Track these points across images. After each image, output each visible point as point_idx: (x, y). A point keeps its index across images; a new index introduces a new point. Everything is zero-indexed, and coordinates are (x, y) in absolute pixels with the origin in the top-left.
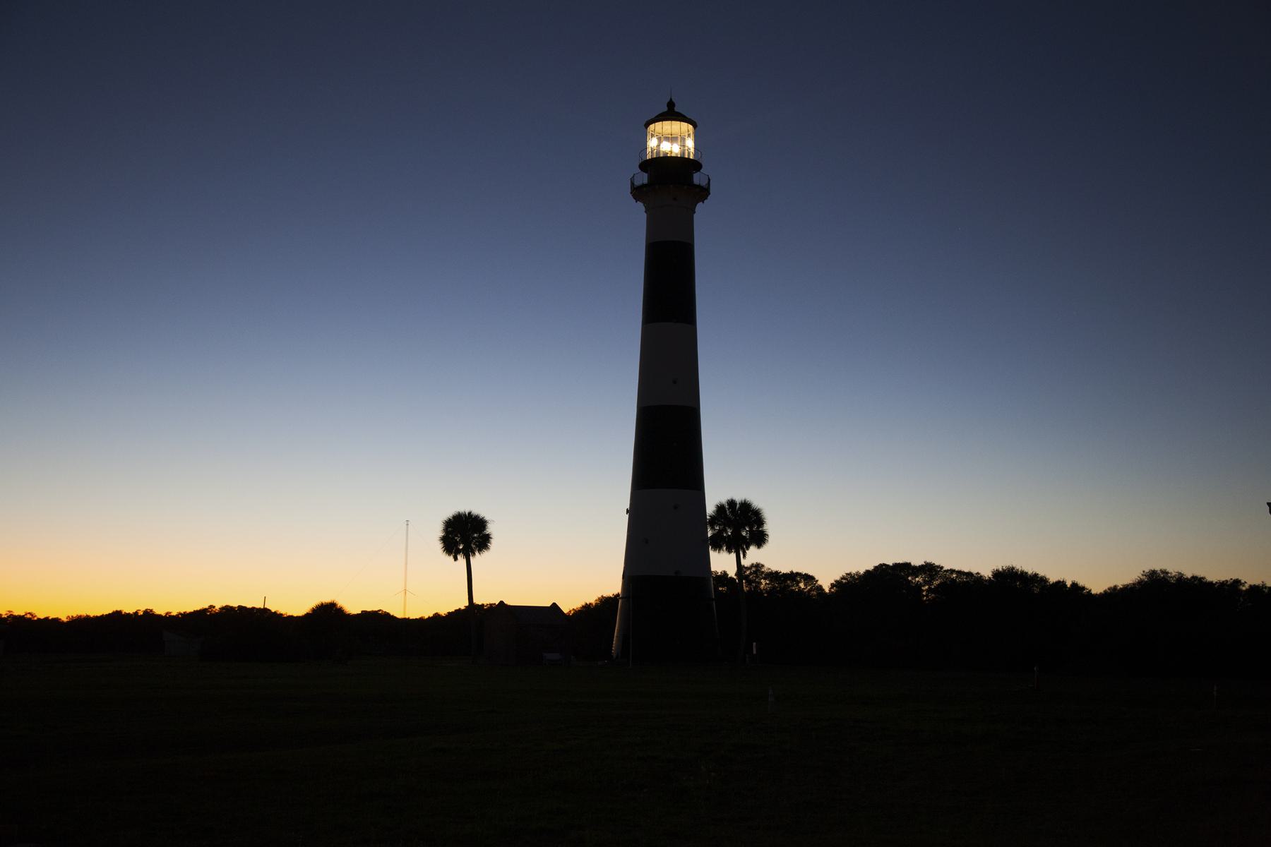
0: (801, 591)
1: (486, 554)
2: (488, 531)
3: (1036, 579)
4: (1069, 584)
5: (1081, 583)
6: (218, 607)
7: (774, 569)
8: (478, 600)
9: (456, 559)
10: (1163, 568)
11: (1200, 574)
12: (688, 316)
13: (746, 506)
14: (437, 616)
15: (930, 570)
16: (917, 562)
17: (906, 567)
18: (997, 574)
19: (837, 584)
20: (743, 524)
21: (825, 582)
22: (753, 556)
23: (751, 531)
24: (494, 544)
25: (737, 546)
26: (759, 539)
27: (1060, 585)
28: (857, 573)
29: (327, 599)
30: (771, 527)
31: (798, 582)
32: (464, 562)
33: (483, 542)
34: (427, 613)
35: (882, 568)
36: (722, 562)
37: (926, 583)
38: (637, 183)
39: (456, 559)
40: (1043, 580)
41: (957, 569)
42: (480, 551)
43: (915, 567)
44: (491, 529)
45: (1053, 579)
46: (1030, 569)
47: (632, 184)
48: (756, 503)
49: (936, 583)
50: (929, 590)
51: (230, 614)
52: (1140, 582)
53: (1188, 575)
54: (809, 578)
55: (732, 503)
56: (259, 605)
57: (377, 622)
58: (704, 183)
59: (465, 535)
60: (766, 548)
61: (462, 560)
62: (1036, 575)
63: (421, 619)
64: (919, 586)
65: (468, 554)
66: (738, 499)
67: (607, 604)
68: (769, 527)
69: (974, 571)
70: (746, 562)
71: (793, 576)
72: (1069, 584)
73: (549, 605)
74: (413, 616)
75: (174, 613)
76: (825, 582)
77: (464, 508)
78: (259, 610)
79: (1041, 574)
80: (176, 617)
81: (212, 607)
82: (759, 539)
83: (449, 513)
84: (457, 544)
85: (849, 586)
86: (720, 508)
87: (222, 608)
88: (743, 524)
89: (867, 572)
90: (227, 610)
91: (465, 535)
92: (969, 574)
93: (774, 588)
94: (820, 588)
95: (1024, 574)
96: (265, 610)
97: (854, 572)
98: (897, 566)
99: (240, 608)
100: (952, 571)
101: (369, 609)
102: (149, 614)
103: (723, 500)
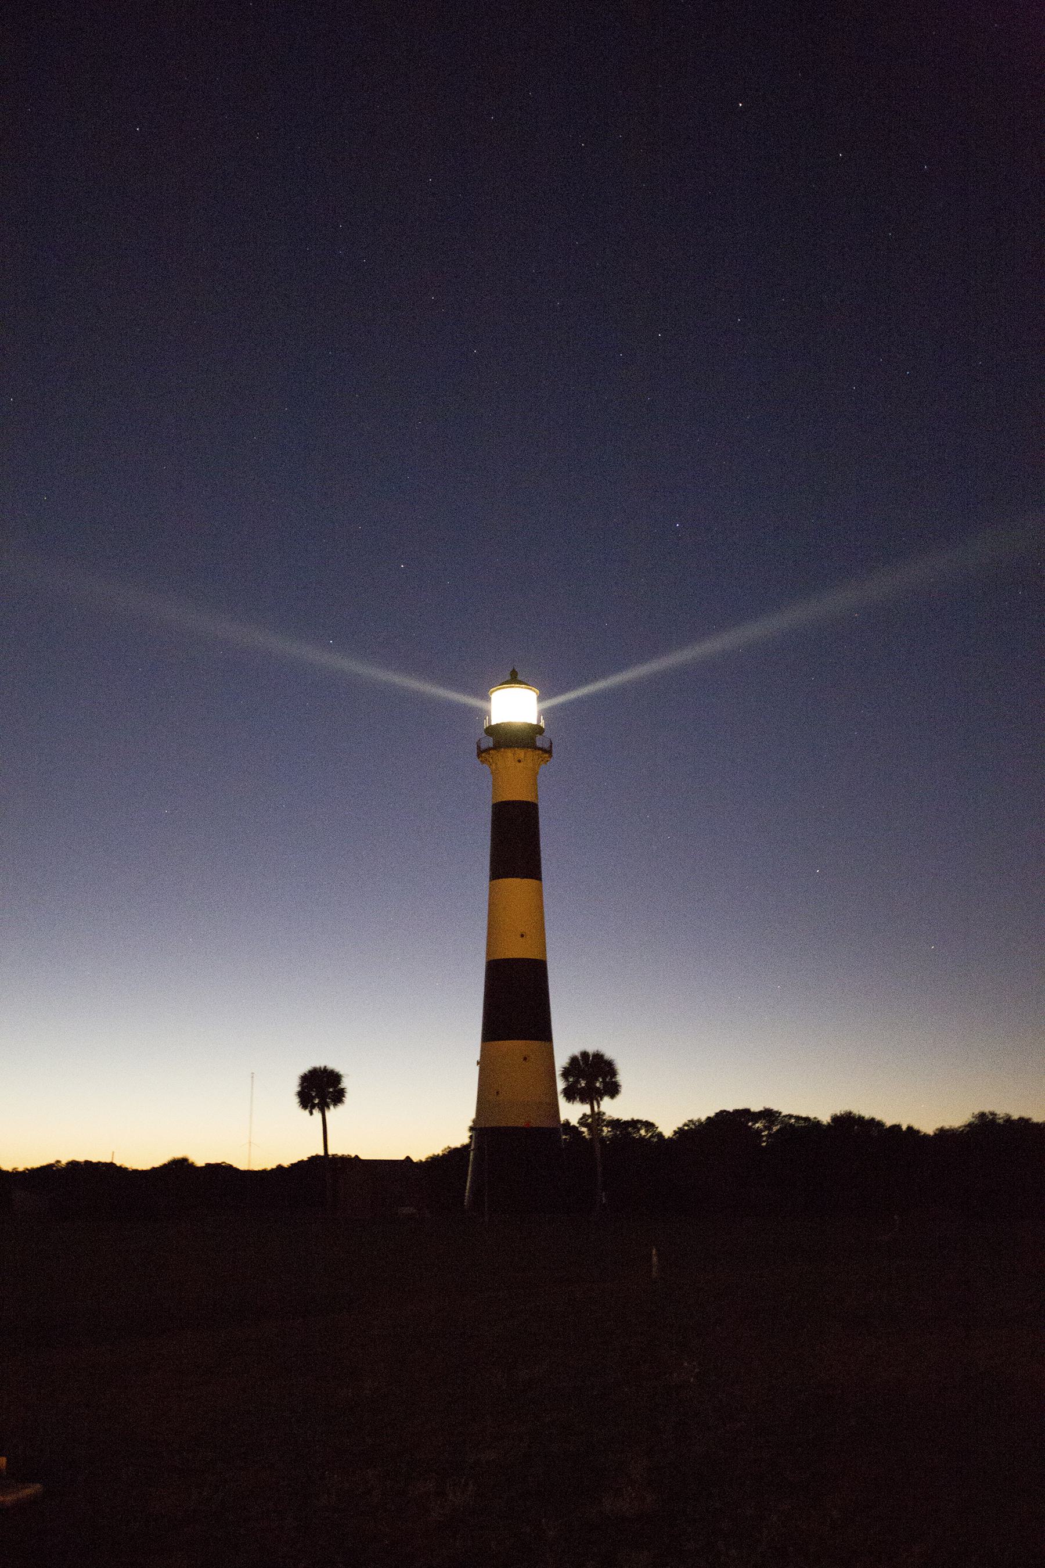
0: (642, 1138)
1: (340, 1107)
2: (343, 1085)
3: (874, 1124)
4: (904, 1128)
5: (916, 1127)
6: (64, 1162)
7: (616, 1116)
8: (331, 1151)
9: (311, 1113)
10: (991, 1109)
11: (1026, 1116)
12: (531, 869)
13: (598, 1057)
14: (280, 1168)
15: (768, 1115)
16: (756, 1107)
17: (746, 1112)
18: (836, 1119)
19: (680, 1132)
20: (595, 1075)
21: (668, 1132)
22: (612, 1108)
23: (604, 1081)
24: (348, 1098)
25: (590, 1096)
26: (613, 1090)
27: (896, 1128)
28: (699, 1120)
29: (179, 1155)
30: (623, 1078)
31: (639, 1130)
32: (320, 1115)
33: (338, 1097)
34: (270, 1165)
35: (722, 1115)
36: (571, 1112)
37: (766, 1128)
38: (483, 746)
39: (311, 1113)
40: (879, 1124)
41: (795, 1113)
42: (335, 1105)
43: (754, 1113)
44: (345, 1083)
45: (889, 1122)
46: (867, 1114)
47: (479, 747)
48: (609, 1054)
49: (775, 1129)
50: (769, 1136)
51: (89, 1167)
52: (970, 1125)
53: (1015, 1116)
54: (649, 1125)
55: (585, 1054)
56: (106, 1159)
57: (220, 1172)
58: (546, 746)
59: (321, 1090)
60: (619, 1098)
61: (317, 1113)
62: (873, 1119)
63: (264, 1171)
64: (759, 1132)
65: (323, 1107)
66: (591, 1049)
67: (455, 1155)
68: (622, 1078)
69: (812, 1116)
70: (586, 1109)
71: (635, 1124)
72: (904, 1128)
73: (402, 1158)
74: (256, 1169)
75: (21, 1169)
76: (668, 1132)
77: (319, 1063)
78: (105, 1164)
79: (878, 1118)
80: (23, 1172)
81: (58, 1162)
82: (613, 1090)
83: (305, 1068)
84: (611, 1143)
85: (693, 1135)
86: (574, 1060)
87: (68, 1164)
88: (595, 1075)
89: (709, 1118)
90: (73, 1165)
91: (321, 1090)
92: (807, 1119)
93: (615, 1135)
94: (660, 1135)
95: (861, 1119)
96: (112, 1164)
97: (695, 1119)
98: (737, 1112)
99: (87, 1162)
100: (790, 1116)
101: (94, 1160)
102: (154, 1168)
103: (576, 1051)
